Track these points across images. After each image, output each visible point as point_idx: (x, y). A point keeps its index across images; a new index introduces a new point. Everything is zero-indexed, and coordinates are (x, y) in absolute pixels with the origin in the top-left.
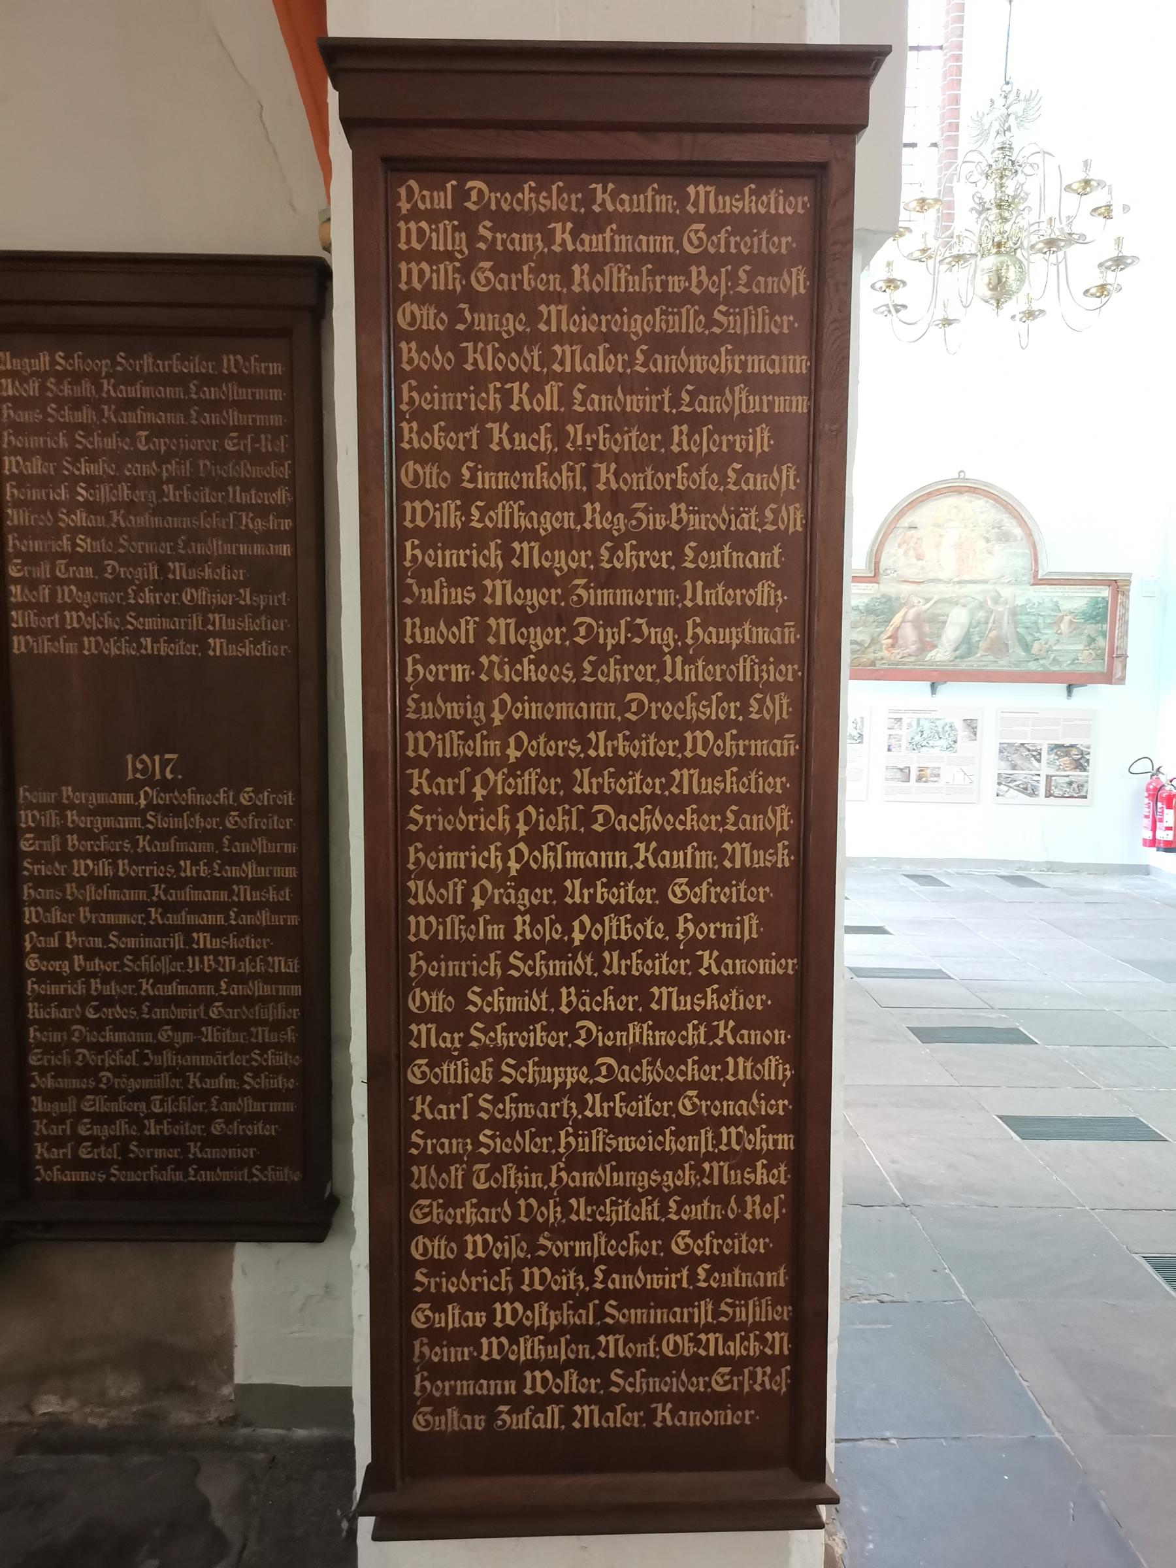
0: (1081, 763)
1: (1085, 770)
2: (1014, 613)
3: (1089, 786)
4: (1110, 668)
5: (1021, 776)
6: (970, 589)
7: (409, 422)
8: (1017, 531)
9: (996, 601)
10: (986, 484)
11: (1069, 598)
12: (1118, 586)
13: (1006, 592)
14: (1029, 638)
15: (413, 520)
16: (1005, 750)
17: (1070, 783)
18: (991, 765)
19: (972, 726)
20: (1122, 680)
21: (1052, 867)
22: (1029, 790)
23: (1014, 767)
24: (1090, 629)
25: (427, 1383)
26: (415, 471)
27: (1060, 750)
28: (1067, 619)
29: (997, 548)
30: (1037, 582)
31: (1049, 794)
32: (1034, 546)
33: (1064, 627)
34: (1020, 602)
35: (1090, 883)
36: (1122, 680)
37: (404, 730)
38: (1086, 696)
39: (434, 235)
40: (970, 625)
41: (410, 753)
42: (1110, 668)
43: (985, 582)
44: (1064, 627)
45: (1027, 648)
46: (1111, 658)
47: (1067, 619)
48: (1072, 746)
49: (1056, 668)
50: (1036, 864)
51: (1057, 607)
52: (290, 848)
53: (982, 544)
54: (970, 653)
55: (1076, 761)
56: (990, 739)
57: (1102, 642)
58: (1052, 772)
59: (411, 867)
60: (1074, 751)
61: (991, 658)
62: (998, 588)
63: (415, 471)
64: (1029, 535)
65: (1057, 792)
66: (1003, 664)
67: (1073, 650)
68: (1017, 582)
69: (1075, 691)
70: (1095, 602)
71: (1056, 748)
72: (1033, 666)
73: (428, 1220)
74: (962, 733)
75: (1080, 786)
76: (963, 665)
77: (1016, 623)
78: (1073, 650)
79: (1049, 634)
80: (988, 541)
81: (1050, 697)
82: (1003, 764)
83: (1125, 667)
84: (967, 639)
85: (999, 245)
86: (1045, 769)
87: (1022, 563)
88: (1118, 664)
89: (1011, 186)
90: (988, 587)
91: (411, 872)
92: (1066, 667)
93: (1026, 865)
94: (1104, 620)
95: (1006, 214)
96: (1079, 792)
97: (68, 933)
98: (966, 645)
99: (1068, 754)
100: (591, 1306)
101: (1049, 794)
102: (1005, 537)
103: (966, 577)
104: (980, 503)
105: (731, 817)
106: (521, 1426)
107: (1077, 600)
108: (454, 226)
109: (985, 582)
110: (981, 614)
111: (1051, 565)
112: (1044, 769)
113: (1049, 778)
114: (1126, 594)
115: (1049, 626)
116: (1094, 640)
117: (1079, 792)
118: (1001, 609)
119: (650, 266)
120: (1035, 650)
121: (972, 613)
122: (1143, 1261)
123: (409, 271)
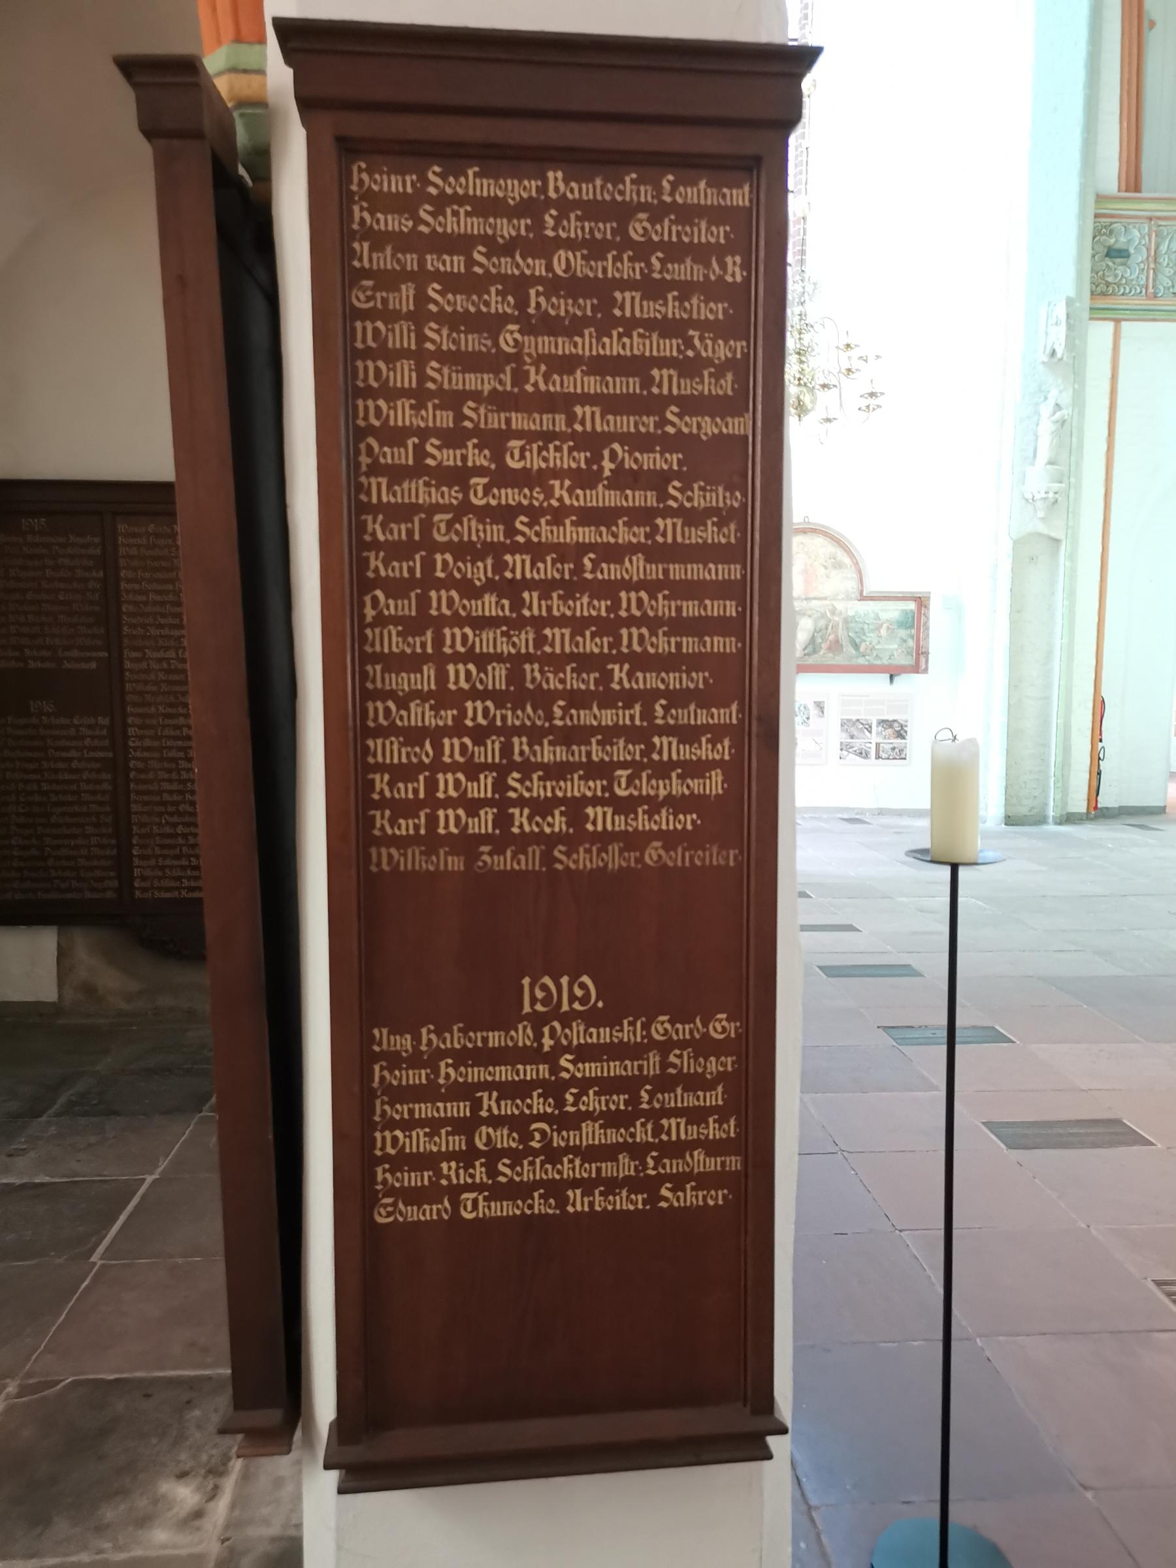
0: (901, 734)
1: (904, 738)
2: (846, 621)
3: (908, 751)
4: (918, 663)
5: (858, 743)
6: (815, 603)
7: (382, 1131)
8: (847, 560)
9: (833, 612)
10: (823, 526)
11: (885, 610)
12: (922, 602)
13: (840, 606)
14: (858, 640)
15: (456, 682)
16: (845, 724)
17: (894, 749)
18: (836, 736)
19: (820, 706)
20: (926, 671)
21: (881, 812)
22: (863, 754)
23: (852, 737)
24: (903, 633)
25: (387, 1107)
26: (488, 1134)
27: (886, 723)
28: (885, 626)
29: (833, 573)
30: (863, 598)
31: (878, 757)
32: (860, 573)
33: (883, 632)
34: (851, 613)
35: (905, 821)
36: (926, 671)
37: (355, 397)
38: (902, 680)
39: (392, 413)
40: (815, 631)
41: (361, 384)
42: (918, 663)
43: (825, 598)
44: (883, 632)
45: (856, 646)
46: (918, 654)
47: (885, 626)
48: (895, 721)
49: (878, 662)
50: (869, 810)
51: (877, 618)
52: (114, 842)
53: (822, 571)
54: (815, 651)
55: (898, 732)
56: (834, 715)
57: (911, 643)
58: (880, 740)
59: (377, 1119)
60: (896, 725)
61: (831, 655)
62: (835, 603)
63: (488, 1134)
64: (856, 564)
65: (884, 755)
66: (839, 660)
67: (894, 650)
68: (848, 598)
69: (896, 679)
70: (905, 612)
71: (883, 723)
72: (861, 661)
73: (371, 304)
74: (814, 712)
75: (901, 751)
76: (810, 661)
77: (848, 629)
78: (894, 650)
79: (871, 637)
80: (826, 568)
81: (877, 684)
82: (844, 735)
83: (927, 661)
84: (813, 640)
85: (799, 379)
86: (874, 738)
87: (852, 585)
88: (923, 660)
89: (807, 338)
90: (827, 602)
91: (377, 1123)
92: (885, 661)
93: (862, 811)
94: (912, 627)
95: (803, 359)
96: (900, 755)
97: (516, 740)
98: (812, 645)
99: (891, 727)
100: (413, 595)
101: (878, 757)
102: (839, 566)
103: (811, 595)
104: (819, 540)
105: (651, 1163)
106: (477, 831)
107: (892, 611)
108: (466, 212)
109: (825, 598)
110: (822, 623)
111: (873, 585)
112: (874, 738)
113: (878, 745)
114: (927, 607)
115: (872, 631)
116: (905, 641)
117: (900, 755)
118: (836, 619)
119: (631, 253)
120: (862, 649)
121: (816, 621)
122: (983, 1127)
123: (453, 636)
